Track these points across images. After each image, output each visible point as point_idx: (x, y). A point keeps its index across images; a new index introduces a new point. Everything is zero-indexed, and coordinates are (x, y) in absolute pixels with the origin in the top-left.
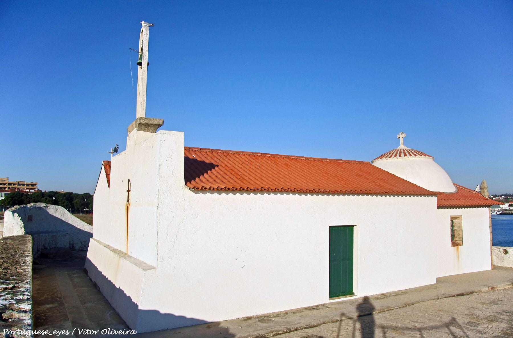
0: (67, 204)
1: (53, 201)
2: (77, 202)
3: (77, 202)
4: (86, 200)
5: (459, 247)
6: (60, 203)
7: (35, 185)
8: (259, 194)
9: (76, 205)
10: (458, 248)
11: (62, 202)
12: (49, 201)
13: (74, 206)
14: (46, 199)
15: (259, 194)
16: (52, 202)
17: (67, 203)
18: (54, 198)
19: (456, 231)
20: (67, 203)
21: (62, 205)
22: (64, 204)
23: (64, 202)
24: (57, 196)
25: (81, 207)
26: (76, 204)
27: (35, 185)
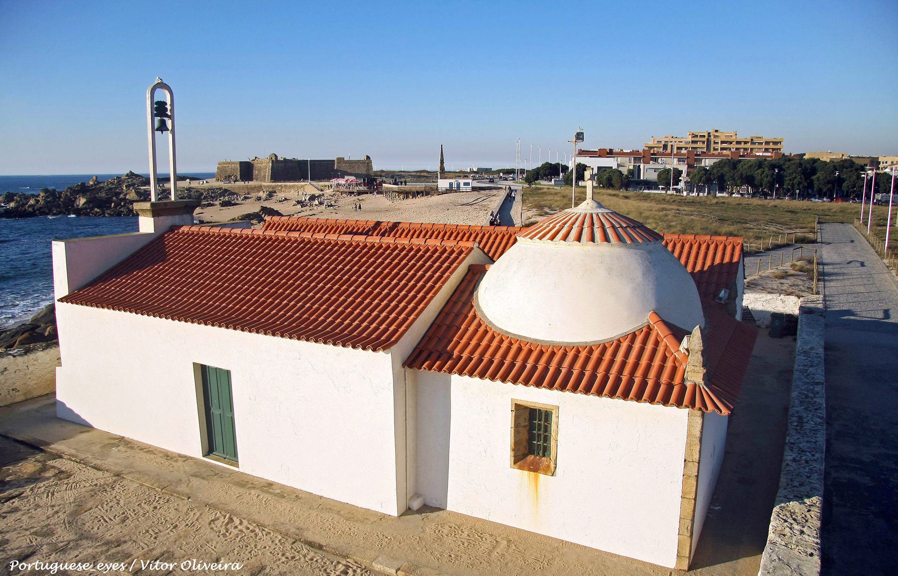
0: (799, 182)
1: (775, 177)
2: (819, 177)
3: (819, 177)
4: (837, 174)
5: (541, 476)
6: (786, 178)
7: (780, 142)
8: (153, 232)
9: (817, 182)
10: (536, 479)
11: (791, 177)
12: (768, 175)
13: (813, 184)
14: (763, 172)
15: (153, 232)
16: (771, 177)
17: (801, 178)
18: (776, 171)
19: (823, 478)
20: (801, 178)
21: (791, 182)
22: (793, 181)
23: (795, 178)
24: (787, 166)
25: (825, 186)
26: (817, 181)
27: (780, 142)
